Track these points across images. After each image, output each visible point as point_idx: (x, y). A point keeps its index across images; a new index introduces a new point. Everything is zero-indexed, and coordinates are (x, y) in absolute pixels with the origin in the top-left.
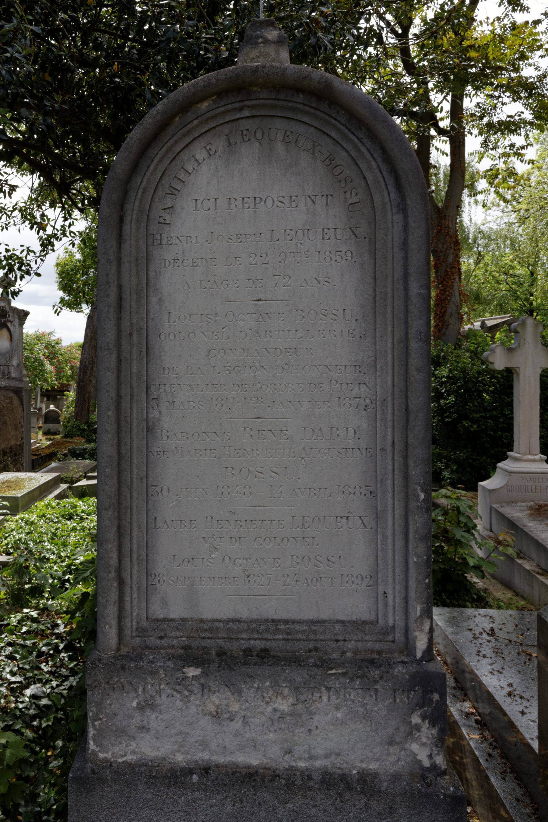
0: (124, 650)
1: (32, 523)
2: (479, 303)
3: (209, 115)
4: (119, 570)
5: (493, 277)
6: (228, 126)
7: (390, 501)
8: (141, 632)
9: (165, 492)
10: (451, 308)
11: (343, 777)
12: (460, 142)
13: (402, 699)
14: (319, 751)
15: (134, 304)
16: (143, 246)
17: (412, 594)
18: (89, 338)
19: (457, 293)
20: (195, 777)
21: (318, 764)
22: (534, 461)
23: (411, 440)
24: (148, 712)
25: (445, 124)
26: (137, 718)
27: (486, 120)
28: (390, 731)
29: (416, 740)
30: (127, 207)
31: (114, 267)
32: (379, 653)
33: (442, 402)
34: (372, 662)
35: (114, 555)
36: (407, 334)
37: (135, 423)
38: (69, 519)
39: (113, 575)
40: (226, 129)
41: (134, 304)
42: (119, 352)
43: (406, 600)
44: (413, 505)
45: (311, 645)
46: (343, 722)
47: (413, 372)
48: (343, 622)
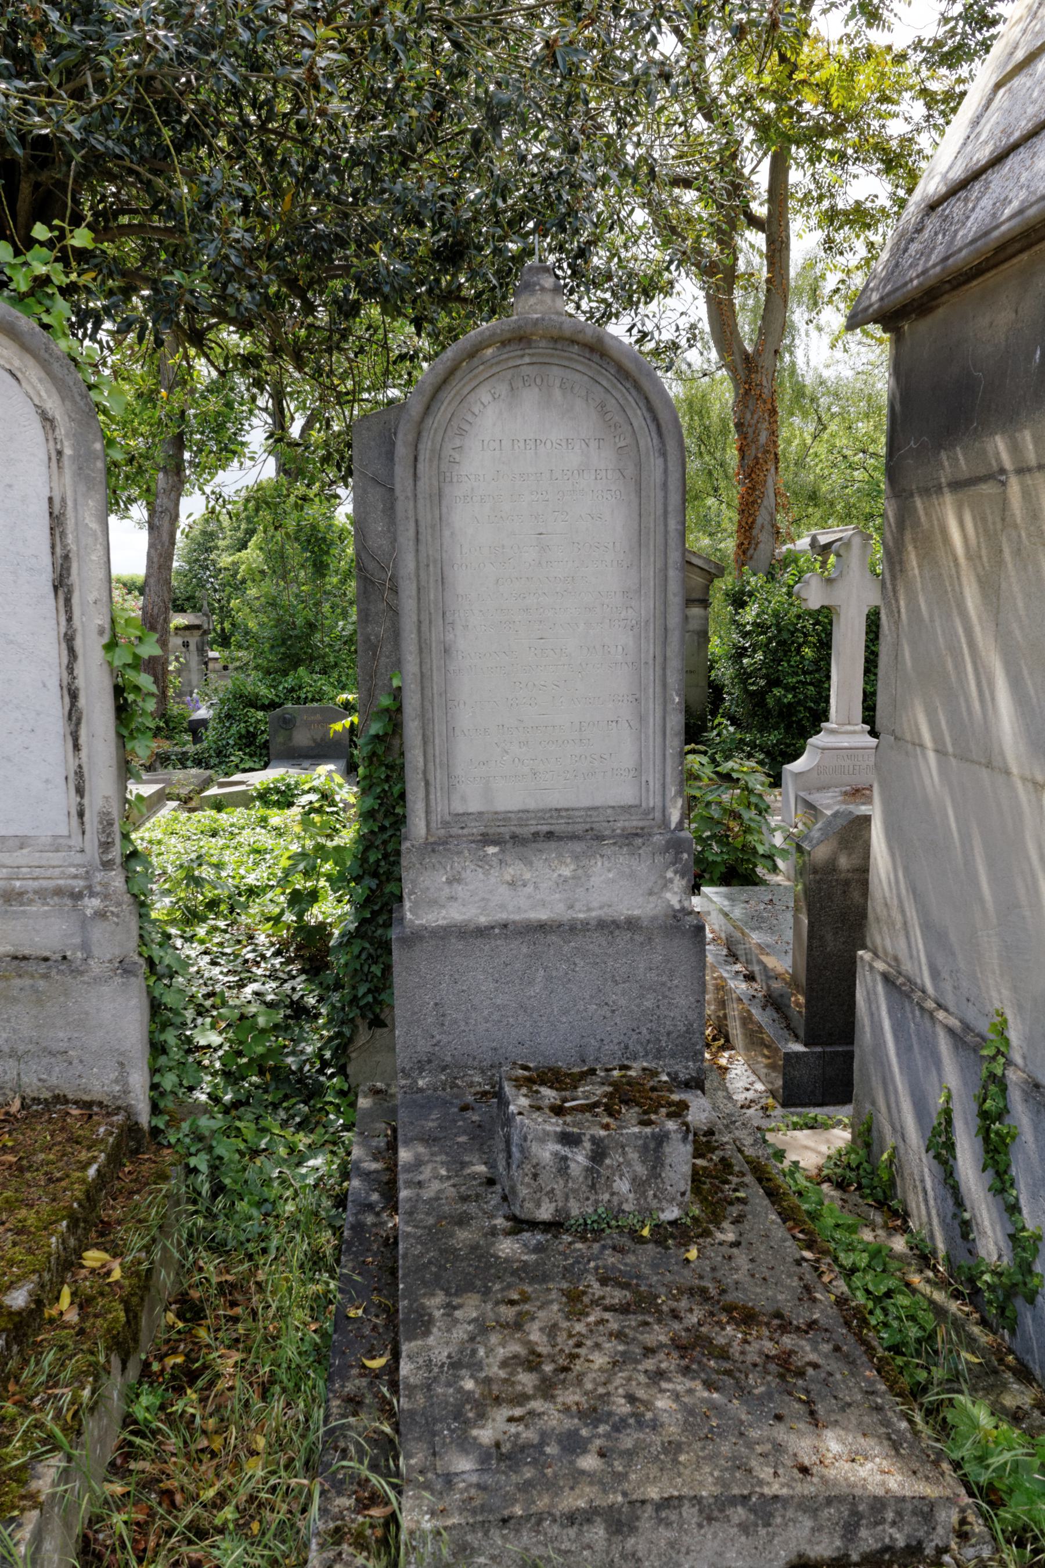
0: (431, 840)
1: (159, 842)
2: (815, 505)
3: (494, 361)
4: (425, 772)
5: (845, 457)
6: (511, 371)
7: (651, 706)
8: (446, 824)
9: (462, 706)
10: (762, 517)
11: (614, 922)
12: (782, 242)
13: (659, 859)
14: (595, 904)
15: (429, 537)
16: (436, 483)
17: (668, 780)
18: (156, 566)
19: (772, 495)
20: (497, 931)
21: (594, 914)
22: (854, 732)
23: (669, 654)
24: (455, 885)
25: (760, 210)
26: (447, 891)
27: (826, 204)
28: (650, 884)
29: (669, 890)
30: (421, 446)
31: (412, 504)
32: (642, 829)
33: (745, 661)
34: (637, 835)
35: (421, 760)
36: (666, 564)
37: (434, 645)
38: (213, 836)
39: (421, 776)
40: (509, 374)
41: (429, 537)
42: (418, 581)
43: (664, 786)
44: (670, 707)
45: (588, 826)
46: (613, 881)
47: (670, 596)
48: (613, 807)
